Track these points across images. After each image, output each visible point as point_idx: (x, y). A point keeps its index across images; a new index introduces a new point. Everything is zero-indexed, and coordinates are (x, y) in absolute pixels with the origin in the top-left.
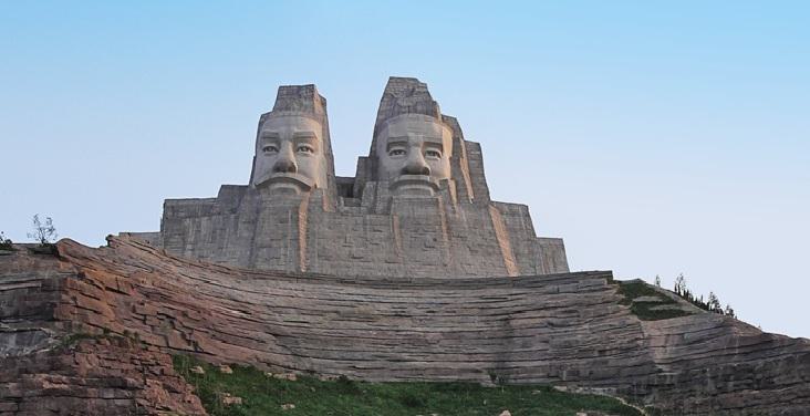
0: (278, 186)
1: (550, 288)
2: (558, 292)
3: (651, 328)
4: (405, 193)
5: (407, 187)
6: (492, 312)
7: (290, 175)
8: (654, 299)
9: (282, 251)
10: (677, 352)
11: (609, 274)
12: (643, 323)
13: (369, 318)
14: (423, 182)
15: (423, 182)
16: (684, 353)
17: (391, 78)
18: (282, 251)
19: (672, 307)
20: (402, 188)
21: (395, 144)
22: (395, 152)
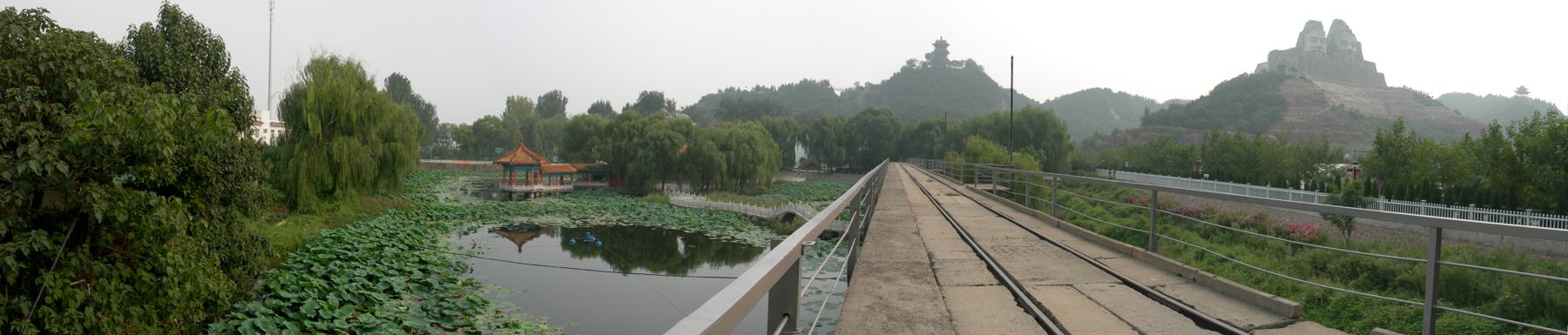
17: (1320, 23)
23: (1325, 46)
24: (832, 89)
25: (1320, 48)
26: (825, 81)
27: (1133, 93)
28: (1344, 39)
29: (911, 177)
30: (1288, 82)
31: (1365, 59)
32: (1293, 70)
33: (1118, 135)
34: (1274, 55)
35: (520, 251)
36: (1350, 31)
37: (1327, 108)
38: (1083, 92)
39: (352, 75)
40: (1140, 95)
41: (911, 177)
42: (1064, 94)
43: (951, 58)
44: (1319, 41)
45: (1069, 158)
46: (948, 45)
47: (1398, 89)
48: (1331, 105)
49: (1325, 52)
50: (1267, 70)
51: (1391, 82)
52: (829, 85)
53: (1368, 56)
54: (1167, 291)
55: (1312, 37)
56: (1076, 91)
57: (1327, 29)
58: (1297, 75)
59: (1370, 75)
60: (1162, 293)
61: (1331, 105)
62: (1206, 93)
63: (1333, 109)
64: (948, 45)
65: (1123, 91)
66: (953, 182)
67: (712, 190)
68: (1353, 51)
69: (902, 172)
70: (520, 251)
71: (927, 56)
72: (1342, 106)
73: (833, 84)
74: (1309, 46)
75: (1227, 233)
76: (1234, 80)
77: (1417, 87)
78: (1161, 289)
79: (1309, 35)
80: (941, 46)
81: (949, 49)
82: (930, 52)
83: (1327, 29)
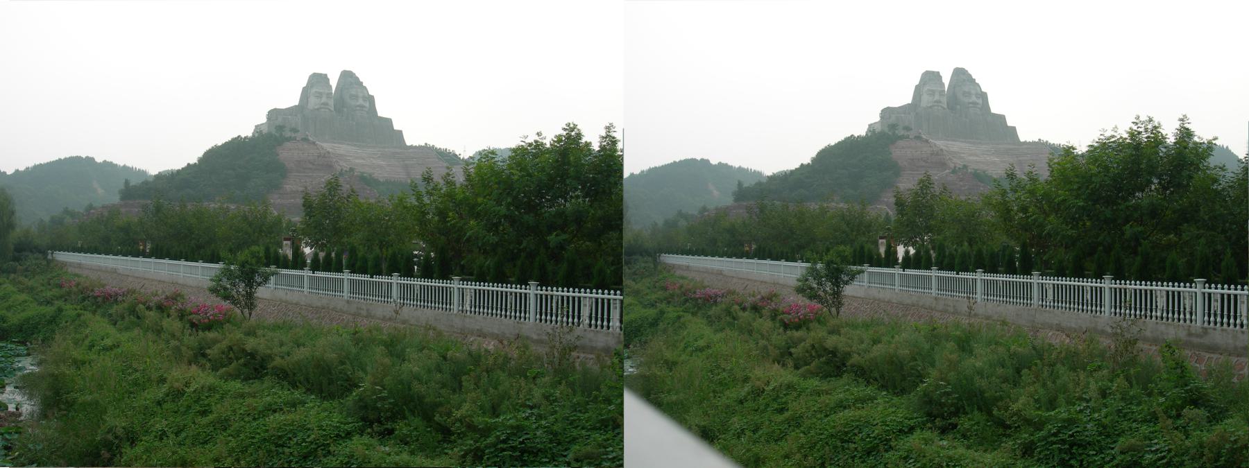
17: (938, 73)
25: (939, 102)
27: (736, 164)
28: (967, 90)
30: (901, 143)
31: (379, 115)
32: (295, 130)
33: (92, 211)
34: (273, 114)
36: (361, 83)
37: (947, 171)
38: (38, 168)
39: (633, 174)
40: (129, 165)
42: (38, 163)
47: (1034, 143)
48: (952, 166)
50: (264, 132)
51: (412, 139)
53: (382, 111)
55: (929, 90)
57: (334, 83)
58: (912, 134)
59: (386, 132)
61: (952, 166)
62: (193, 160)
63: (954, 171)
65: (109, 160)
67: (285, 302)
68: (364, 107)
72: (352, 170)
74: (313, 102)
76: (226, 144)
77: (440, 144)
79: (314, 90)
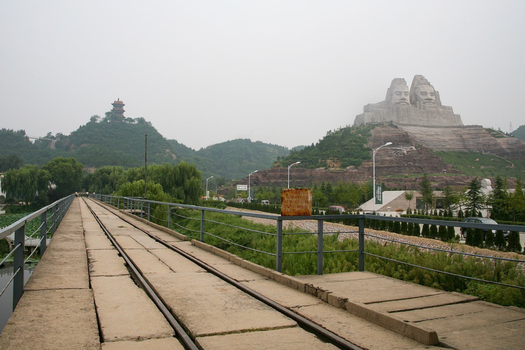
0: (402, 103)
1: (468, 129)
2: (470, 130)
3: (499, 140)
4: (427, 105)
5: (428, 103)
6: (456, 134)
7: (405, 101)
8: (495, 133)
9: (405, 118)
10: (508, 146)
11: (481, 126)
12: (496, 139)
13: (432, 136)
14: (404, 102)
15: (404, 102)
16: (510, 147)
17: (404, 79)
18: (405, 118)
19: (501, 135)
20: (426, 103)
21: (423, 93)
22: (423, 95)
23: (408, 98)
24: (27, 138)
26: (22, 131)
29: (88, 206)
35: (2, 277)
41: (88, 206)
43: (126, 115)
44: (403, 94)
45: (88, 178)
46: (124, 105)
49: (409, 102)
52: (25, 134)
54: (304, 311)
56: (219, 142)
60: (297, 313)
64: (124, 105)
66: (114, 208)
69: (83, 204)
70: (2, 277)
71: (108, 114)
73: (28, 134)
75: (250, 250)
78: (296, 309)
80: (118, 106)
81: (124, 108)
82: (109, 111)
83: (409, 84)
